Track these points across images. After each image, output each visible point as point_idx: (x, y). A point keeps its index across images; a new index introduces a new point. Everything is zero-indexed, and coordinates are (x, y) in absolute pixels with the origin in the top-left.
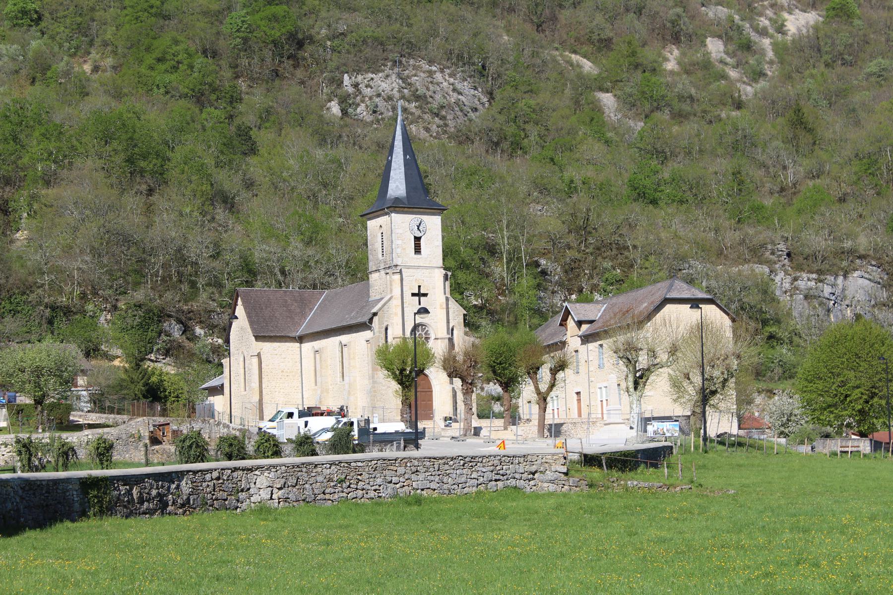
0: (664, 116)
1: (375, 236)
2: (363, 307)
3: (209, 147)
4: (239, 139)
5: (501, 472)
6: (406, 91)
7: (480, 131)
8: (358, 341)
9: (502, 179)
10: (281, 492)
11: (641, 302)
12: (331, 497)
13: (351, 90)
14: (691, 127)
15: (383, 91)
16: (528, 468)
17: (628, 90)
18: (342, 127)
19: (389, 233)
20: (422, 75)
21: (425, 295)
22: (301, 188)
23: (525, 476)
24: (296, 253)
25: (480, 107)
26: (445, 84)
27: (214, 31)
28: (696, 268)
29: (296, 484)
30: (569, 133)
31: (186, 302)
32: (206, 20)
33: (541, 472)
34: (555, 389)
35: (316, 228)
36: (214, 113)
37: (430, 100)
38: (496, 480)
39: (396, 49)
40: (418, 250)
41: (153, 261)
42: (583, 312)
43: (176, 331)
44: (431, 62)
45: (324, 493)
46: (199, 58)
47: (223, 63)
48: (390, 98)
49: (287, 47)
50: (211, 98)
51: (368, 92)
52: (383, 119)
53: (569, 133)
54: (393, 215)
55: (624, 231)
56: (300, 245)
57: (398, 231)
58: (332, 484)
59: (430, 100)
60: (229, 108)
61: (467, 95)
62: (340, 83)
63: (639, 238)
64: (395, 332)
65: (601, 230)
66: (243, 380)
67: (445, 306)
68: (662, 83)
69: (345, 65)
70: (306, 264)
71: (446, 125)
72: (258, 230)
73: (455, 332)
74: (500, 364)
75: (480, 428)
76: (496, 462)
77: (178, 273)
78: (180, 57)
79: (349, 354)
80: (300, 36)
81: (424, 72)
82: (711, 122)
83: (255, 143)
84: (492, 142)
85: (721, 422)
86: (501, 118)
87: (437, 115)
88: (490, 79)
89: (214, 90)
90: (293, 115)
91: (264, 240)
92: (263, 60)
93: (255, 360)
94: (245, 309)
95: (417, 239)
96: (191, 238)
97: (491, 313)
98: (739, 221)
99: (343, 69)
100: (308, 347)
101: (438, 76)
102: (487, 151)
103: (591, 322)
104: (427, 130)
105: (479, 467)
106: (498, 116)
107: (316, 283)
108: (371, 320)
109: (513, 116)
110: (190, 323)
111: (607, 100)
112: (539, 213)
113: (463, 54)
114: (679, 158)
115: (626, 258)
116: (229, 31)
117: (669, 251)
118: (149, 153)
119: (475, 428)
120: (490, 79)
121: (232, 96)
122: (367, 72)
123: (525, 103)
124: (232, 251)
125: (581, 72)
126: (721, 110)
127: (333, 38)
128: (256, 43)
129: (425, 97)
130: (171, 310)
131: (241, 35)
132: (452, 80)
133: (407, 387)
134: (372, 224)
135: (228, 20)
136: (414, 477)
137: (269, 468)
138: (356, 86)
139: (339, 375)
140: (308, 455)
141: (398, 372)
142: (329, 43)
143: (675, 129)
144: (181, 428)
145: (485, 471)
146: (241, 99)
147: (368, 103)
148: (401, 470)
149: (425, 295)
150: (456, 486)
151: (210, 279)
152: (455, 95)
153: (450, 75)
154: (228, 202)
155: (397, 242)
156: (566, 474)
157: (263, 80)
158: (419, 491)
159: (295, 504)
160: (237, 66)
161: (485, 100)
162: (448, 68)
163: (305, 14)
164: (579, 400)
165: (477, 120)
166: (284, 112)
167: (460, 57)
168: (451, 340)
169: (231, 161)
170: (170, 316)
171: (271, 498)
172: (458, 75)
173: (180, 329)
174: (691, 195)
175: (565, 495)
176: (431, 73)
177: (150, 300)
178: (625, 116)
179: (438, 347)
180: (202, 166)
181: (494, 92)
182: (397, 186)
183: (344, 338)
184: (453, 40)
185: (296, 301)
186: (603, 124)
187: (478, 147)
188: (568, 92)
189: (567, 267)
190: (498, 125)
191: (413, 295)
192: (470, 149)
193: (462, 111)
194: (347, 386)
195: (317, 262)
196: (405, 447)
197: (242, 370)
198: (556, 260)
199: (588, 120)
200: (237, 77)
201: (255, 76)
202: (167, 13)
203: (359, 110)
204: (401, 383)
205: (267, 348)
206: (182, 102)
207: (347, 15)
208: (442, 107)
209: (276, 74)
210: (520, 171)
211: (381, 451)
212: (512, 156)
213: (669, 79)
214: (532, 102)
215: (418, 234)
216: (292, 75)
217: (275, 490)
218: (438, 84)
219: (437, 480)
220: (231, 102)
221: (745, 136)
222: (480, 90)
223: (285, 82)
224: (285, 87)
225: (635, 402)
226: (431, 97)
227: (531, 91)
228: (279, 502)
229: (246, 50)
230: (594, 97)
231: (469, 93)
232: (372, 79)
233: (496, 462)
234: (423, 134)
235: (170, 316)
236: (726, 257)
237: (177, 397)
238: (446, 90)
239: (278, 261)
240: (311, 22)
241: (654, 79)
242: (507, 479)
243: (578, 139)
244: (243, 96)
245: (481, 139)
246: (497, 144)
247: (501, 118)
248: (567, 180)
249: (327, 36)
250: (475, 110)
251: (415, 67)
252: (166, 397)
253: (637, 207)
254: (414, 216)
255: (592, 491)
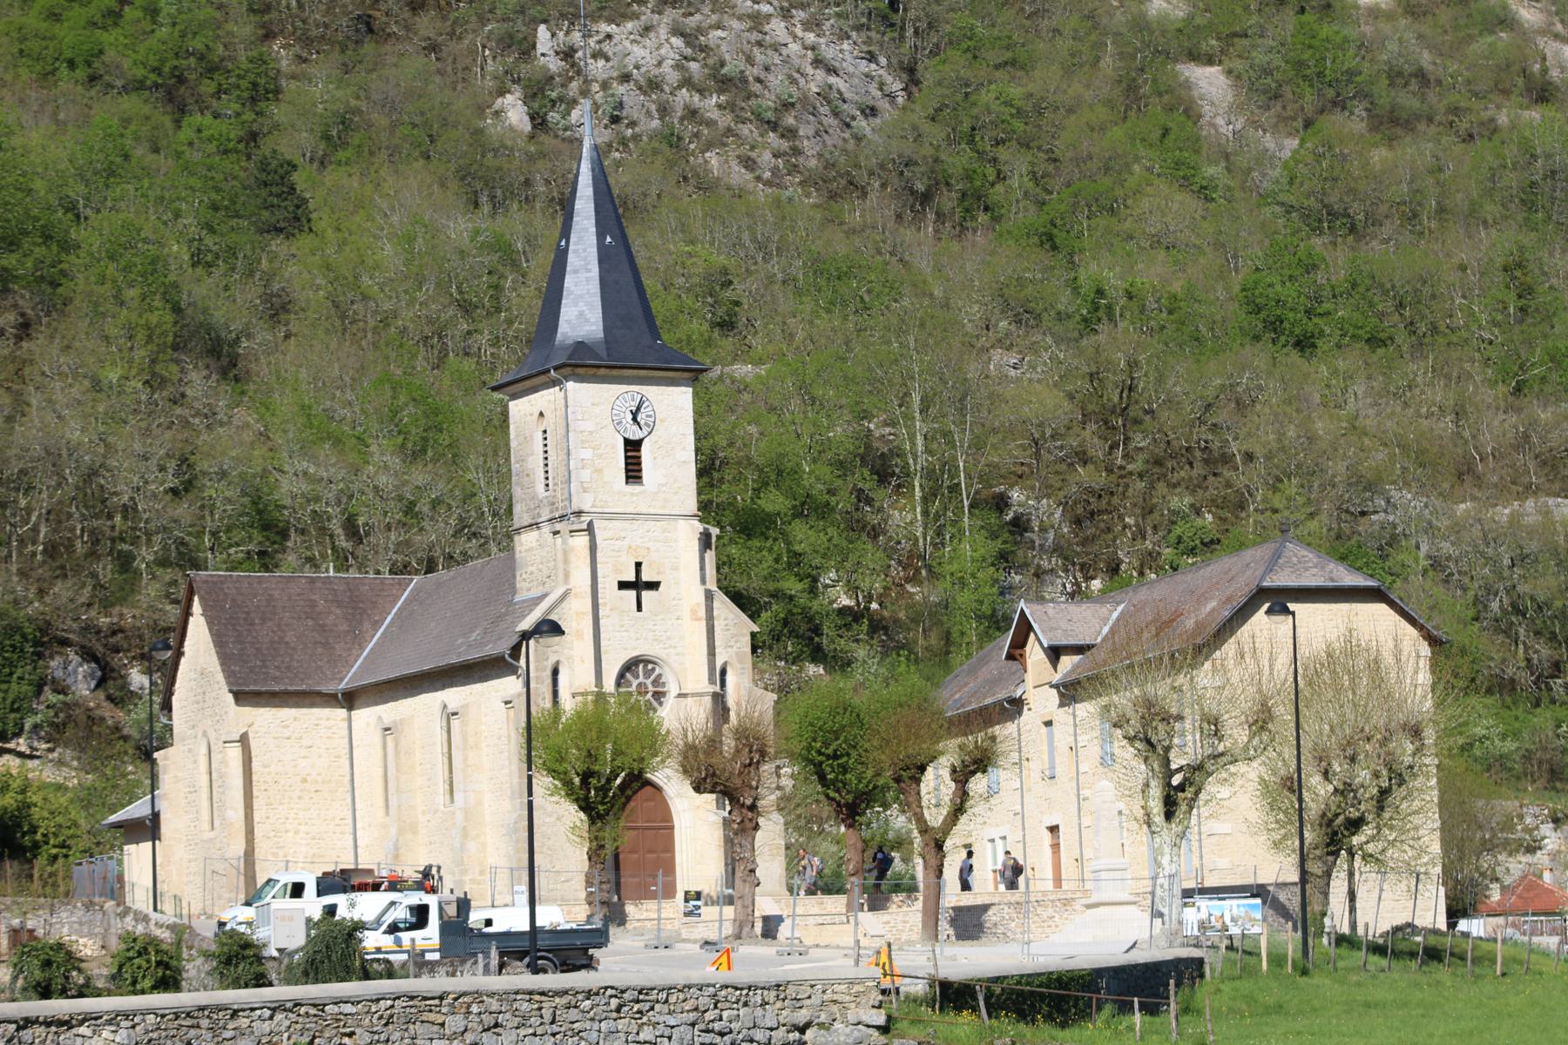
0: (1355, 122)
1: (528, 440)
2: (501, 617)
5: (717, 1026)
7: (882, 166)
8: (490, 706)
11: (1202, 599)
13: (554, 65)
14: (1417, 151)
15: (637, 67)
17: (1260, 57)
19: (562, 431)
20: (735, 24)
21: (653, 586)
22: (406, 317)
24: (382, 480)
25: (883, 104)
26: (794, 47)
28: (1406, 508)
30: (1107, 169)
31: (106, 606)
33: (821, 1025)
34: (963, 819)
37: (756, 87)
40: (633, 472)
41: (23, 503)
42: (1063, 625)
43: (81, 680)
48: (654, 85)
50: (203, 89)
51: (598, 68)
52: (636, 138)
53: (1107, 169)
54: (570, 385)
55: (1222, 416)
56: (395, 462)
57: (580, 425)
59: (756, 87)
60: (248, 116)
61: (850, 75)
62: (527, 49)
63: (1259, 433)
65: (1164, 414)
66: (205, 804)
67: (702, 612)
68: (1346, 40)
70: (410, 509)
71: (797, 151)
73: (730, 678)
74: (835, 757)
76: (704, 1001)
79: (465, 739)
81: (740, 18)
82: (1471, 136)
83: (306, 201)
84: (913, 192)
85: (1392, 895)
87: (773, 126)
88: (910, 32)
89: (211, 70)
90: (406, 130)
91: (305, 450)
93: (235, 752)
94: (210, 624)
95: (633, 446)
96: (121, 445)
98: (1518, 390)
100: (367, 717)
101: (777, 28)
102: (899, 217)
103: (1079, 649)
104: (749, 163)
105: (660, 1014)
106: (926, 127)
107: (379, 564)
109: (966, 127)
110: (120, 659)
111: (1209, 83)
112: (1012, 373)
114: (1387, 230)
115: (1228, 485)
117: (1338, 469)
118: (26, 233)
119: (766, 919)
120: (910, 32)
121: (255, 85)
122: (595, 17)
123: (999, 93)
125: (1143, 15)
126: (1498, 107)
129: (744, 80)
130: (67, 626)
132: (811, 37)
134: (521, 410)
137: (114, 1019)
138: (568, 54)
139: (442, 787)
140: (246, 986)
141: (577, 780)
143: (1379, 156)
144: (30, 924)
146: (277, 91)
147: (599, 97)
148: (455, 1023)
149: (653, 586)
151: (165, 548)
152: (820, 74)
153: (807, 26)
154: (224, 358)
155: (581, 454)
157: (332, 43)
161: (896, 86)
164: (1056, 847)
165: (876, 138)
168: (719, 699)
169: (232, 252)
170: (65, 643)
173: (92, 675)
174: (1395, 325)
177: (16, 602)
178: (1255, 124)
179: (682, 714)
180: (153, 262)
181: (920, 67)
182: (582, 313)
183: (453, 696)
185: (339, 603)
186: (1195, 144)
188: (1108, 63)
189: (1080, 510)
190: (927, 150)
191: (623, 585)
193: (836, 114)
194: (459, 815)
195: (435, 504)
196: (502, 966)
197: (205, 779)
198: (1047, 491)
199: (1156, 135)
200: (269, 36)
201: (314, 32)
203: (575, 114)
204: (586, 806)
205: (265, 721)
206: (131, 104)
208: (788, 106)
210: (960, 269)
211: (453, 975)
212: (963, 228)
213: (1367, 29)
214: (1015, 92)
215: (634, 433)
216: (407, 28)
218: (776, 47)
221: (1553, 172)
222: (883, 61)
223: (388, 48)
224: (390, 59)
225: (1167, 850)
226: (759, 80)
227: (1013, 63)
230: (1176, 75)
231: (857, 70)
232: (609, 36)
233: (704, 1001)
235: (65, 643)
236: (1479, 481)
237: (63, 846)
239: (339, 503)
241: (1326, 30)
243: (1132, 182)
244: (283, 83)
245: (884, 186)
246: (926, 198)
248: (1087, 288)
250: (871, 111)
252: (36, 846)
253: (1259, 356)
254: (624, 388)
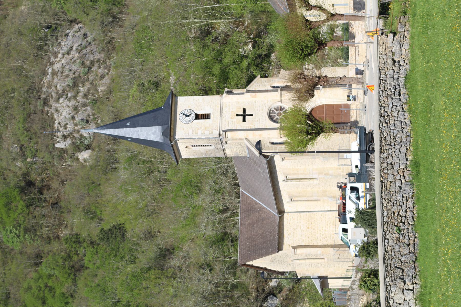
2: (255, 162)
3: (118, 268)
4: (111, 239)
5: (393, 90)
6: (69, 95)
7: (104, 32)
8: (285, 165)
9: (145, 19)
10: (407, 282)
12: (412, 239)
13: (69, 142)
15: (70, 114)
16: (390, 67)
18: (100, 150)
19: (192, 140)
20: (55, 81)
21: (244, 110)
23: (396, 69)
24: (208, 200)
25: (83, 31)
26: (63, 61)
27: (19, 256)
29: (401, 269)
31: (249, 293)
32: (10, 263)
33: (393, 55)
35: (188, 183)
36: (89, 257)
37: (77, 74)
38: (400, 95)
39: (33, 102)
40: (206, 117)
44: (45, 73)
45: (409, 245)
46: (42, 269)
47: (46, 250)
48: (76, 109)
49: (32, 196)
51: (70, 127)
52: (93, 115)
54: (177, 137)
58: (401, 238)
59: (77, 74)
61: (73, 42)
62: (63, 151)
64: (275, 136)
66: (315, 261)
67: (254, 94)
69: (47, 147)
71: (98, 61)
72: (189, 231)
73: (275, 85)
74: (302, 50)
75: (357, 69)
76: (384, 94)
77: (224, 298)
78: (42, 285)
80: (23, 184)
81: (53, 79)
83: (114, 226)
84: (112, 22)
86: (93, 14)
87: (90, 68)
88: (58, 22)
89: (69, 257)
92: (44, 216)
93: (298, 251)
94: (255, 259)
95: (198, 117)
97: (259, 35)
99: (51, 149)
100: (287, 206)
101: (57, 67)
102: (121, 26)
104: (102, 77)
105: (388, 109)
106: (91, 17)
107: (236, 202)
108: (266, 157)
110: (267, 290)
113: (37, 45)
116: (18, 244)
119: (357, 74)
120: (58, 22)
121: (74, 242)
122: (53, 128)
124: (205, 254)
127: (24, 156)
128: (29, 222)
129: (74, 78)
131: (22, 233)
132: (60, 55)
133: (322, 129)
134: (185, 154)
135: (10, 245)
136: (396, 167)
137: (387, 292)
138: (65, 137)
139: (311, 182)
140: (377, 248)
141: (309, 137)
142: (29, 160)
145: (392, 105)
146: (77, 235)
148: (390, 178)
149: (244, 110)
150: (404, 130)
152: (72, 52)
153: (56, 56)
154: (166, 253)
155: (200, 134)
156: (395, 34)
157: (61, 216)
158: (408, 163)
159: (417, 270)
160: (49, 238)
161: (76, 27)
162: (49, 58)
163: (5, 179)
166: (87, 199)
167: (40, 48)
168: (283, 89)
169: (131, 250)
171: (413, 290)
172: (56, 50)
173: (272, 298)
175: (412, 37)
176: (54, 73)
179: (288, 101)
181: (70, 19)
182: (153, 133)
183: (280, 178)
184: (26, 54)
185: (249, 215)
187: (117, 34)
191: (244, 120)
192: (120, 41)
195: (216, 183)
196: (372, 162)
197: (307, 261)
201: (57, 222)
202: (4, 295)
203: (85, 135)
204: (318, 134)
205: (288, 241)
206: (80, 284)
207: (5, 143)
208: (83, 64)
209: (55, 204)
211: (374, 178)
215: (193, 116)
216: (56, 191)
217: (406, 287)
218: (63, 67)
219: (399, 147)
220: (80, 243)
222: (68, 31)
224: (66, 197)
226: (74, 73)
228: (416, 283)
229: (35, 230)
231: (71, 40)
232: (59, 123)
233: (384, 94)
234: (106, 80)
238: (68, 60)
239: (215, 215)
240: (11, 175)
242: (399, 85)
244: (74, 232)
245: (110, 31)
246: (114, 17)
247: (93, 14)
249: (22, 161)
250: (85, 35)
251: (49, 87)
254: (178, 119)
255: (409, 12)
